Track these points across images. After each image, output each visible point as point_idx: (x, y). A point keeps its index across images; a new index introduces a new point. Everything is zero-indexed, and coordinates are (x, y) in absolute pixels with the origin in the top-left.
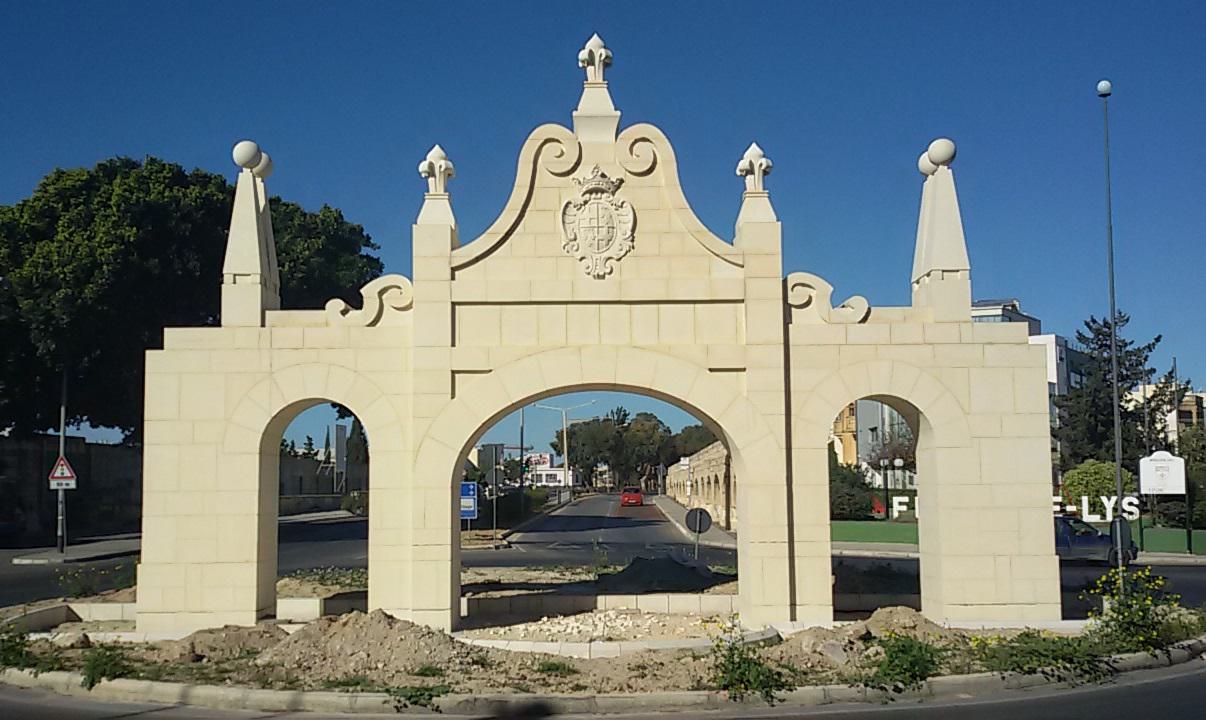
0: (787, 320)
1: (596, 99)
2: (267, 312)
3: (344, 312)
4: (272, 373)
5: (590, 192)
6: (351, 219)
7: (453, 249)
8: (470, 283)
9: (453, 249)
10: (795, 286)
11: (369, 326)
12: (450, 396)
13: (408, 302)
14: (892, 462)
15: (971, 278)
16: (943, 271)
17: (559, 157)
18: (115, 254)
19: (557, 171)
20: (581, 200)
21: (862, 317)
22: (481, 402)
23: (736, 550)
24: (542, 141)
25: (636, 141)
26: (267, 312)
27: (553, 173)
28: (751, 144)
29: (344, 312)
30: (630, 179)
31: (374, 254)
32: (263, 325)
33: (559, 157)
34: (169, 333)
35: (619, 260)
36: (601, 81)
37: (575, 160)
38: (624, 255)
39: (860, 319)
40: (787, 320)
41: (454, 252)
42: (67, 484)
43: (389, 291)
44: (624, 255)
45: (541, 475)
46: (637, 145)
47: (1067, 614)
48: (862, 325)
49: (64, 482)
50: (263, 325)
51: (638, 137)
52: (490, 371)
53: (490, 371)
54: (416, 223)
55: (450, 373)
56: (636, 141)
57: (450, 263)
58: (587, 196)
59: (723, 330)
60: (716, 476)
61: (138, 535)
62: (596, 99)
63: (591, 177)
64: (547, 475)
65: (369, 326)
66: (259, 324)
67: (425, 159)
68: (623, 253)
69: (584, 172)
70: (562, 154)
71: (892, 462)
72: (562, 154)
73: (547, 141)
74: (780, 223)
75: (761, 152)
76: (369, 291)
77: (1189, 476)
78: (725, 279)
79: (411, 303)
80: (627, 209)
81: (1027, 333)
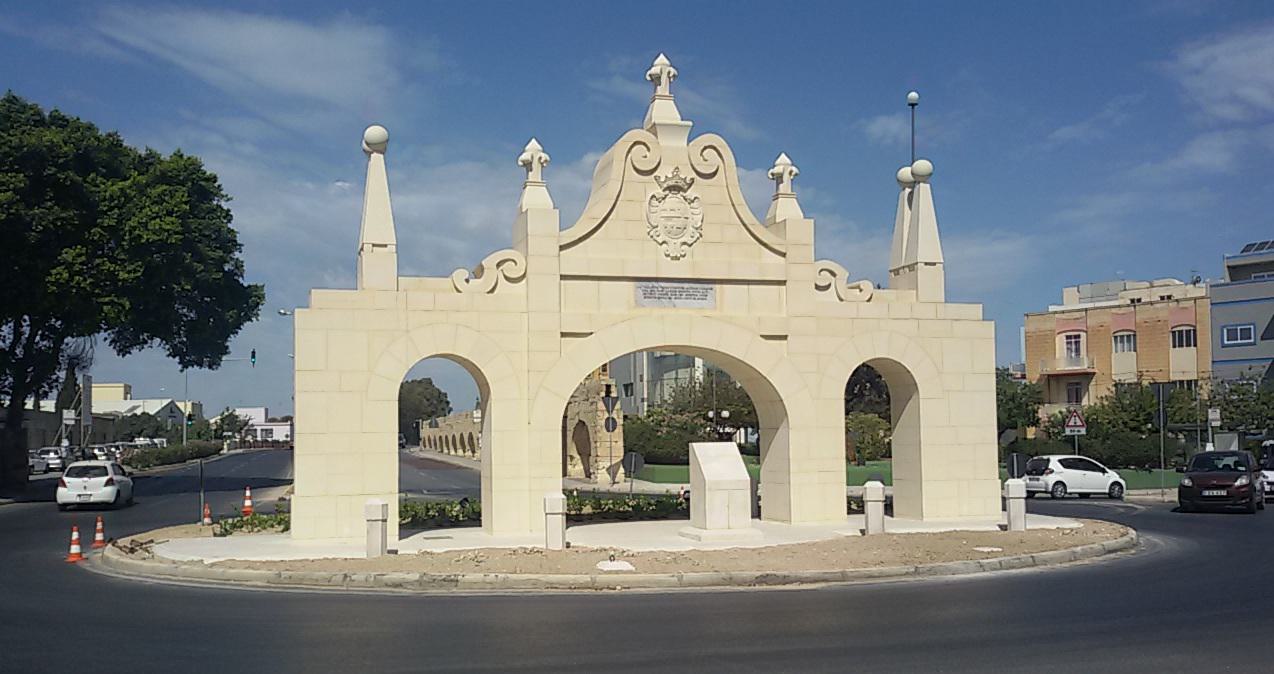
1: (664, 110)
4: (408, 331)
5: (670, 188)
6: (209, 168)
8: (576, 260)
9: (560, 230)
11: (488, 293)
13: (827, 283)
14: (718, 414)
15: (397, 252)
16: (374, 245)
18: (11, 204)
19: (638, 166)
20: (663, 194)
23: (848, 485)
27: (634, 166)
31: (225, 205)
35: (690, 245)
36: (667, 93)
42: (1079, 431)
43: (507, 263)
45: (256, 430)
48: (490, 295)
49: (1076, 429)
51: (707, 144)
52: (591, 333)
53: (591, 333)
56: (705, 148)
57: (559, 241)
58: (667, 192)
60: (462, 435)
61: (1016, 474)
62: (664, 110)
64: (262, 430)
65: (488, 293)
68: (695, 239)
70: (646, 157)
71: (718, 414)
72: (646, 157)
73: (636, 143)
74: (558, 211)
75: (540, 148)
77: (1001, 421)
78: (772, 265)
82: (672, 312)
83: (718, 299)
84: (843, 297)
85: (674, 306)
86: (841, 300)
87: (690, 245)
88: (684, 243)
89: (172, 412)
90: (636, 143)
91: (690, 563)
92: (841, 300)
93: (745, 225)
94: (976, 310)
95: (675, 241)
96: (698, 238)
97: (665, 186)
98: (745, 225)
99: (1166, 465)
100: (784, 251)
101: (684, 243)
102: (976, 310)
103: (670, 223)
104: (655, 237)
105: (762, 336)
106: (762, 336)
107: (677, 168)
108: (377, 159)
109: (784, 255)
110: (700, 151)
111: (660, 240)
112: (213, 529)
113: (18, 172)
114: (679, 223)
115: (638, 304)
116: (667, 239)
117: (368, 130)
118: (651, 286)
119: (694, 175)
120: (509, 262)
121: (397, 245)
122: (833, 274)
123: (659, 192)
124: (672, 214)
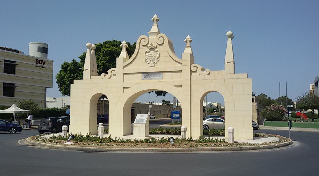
0: (191, 75)
1: (155, 29)
2: (91, 76)
3: (105, 76)
7: (124, 62)
10: (194, 67)
12: (123, 92)
13: (115, 74)
16: (227, 62)
17: (144, 42)
18: (104, 63)
20: (149, 50)
21: (208, 73)
22: (129, 93)
24: (141, 39)
25: (160, 37)
26: (91, 76)
28: (188, 35)
29: (105, 76)
30: (158, 46)
32: (90, 79)
33: (144, 42)
34: (75, 81)
35: (156, 63)
37: (147, 42)
38: (157, 62)
39: (208, 74)
40: (191, 75)
41: (124, 63)
44: (157, 62)
46: (142, 40)
47: (256, 136)
48: (208, 75)
50: (90, 79)
51: (160, 36)
54: (183, 53)
55: (181, 85)
56: (160, 37)
59: (177, 78)
62: (155, 29)
63: (150, 46)
65: (109, 78)
66: (233, 73)
67: (186, 39)
68: (157, 61)
69: (149, 45)
73: (142, 39)
76: (109, 71)
78: (178, 67)
79: (116, 75)
80: (158, 54)
81: (73, 84)
82: (151, 81)
83: (163, 77)
84: (200, 74)
85: (152, 79)
86: (200, 75)
87: (156, 63)
88: (154, 63)
89: (211, 105)
90: (142, 39)
91: (48, 139)
92: (200, 75)
93: (170, 56)
94: (245, 75)
95: (152, 62)
96: (158, 61)
97: (149, 48)
98: (170, 56)
99: (177, 123)
100: (181, 62)
101: (154, 63)
102: (245, 75)
103: (150, 58)
104: (147, 62)
105: (174, 86)
106: (174, 86)
107: (151, 44)
108: (229, 40)
109: (181, 63)
110: (158, 39)
111: (148, 62)
112: (106, 131)
113: (107, 56)
114: (153, 58)
115: (143, 79)
116: (150, 62)
117: (227, 33)
118: (146, 74)
119: (157, 45)
120: (113, 71)
121: (90, 69)
122: (197, 67)
123: (149, 50)
124: (151, 55)
